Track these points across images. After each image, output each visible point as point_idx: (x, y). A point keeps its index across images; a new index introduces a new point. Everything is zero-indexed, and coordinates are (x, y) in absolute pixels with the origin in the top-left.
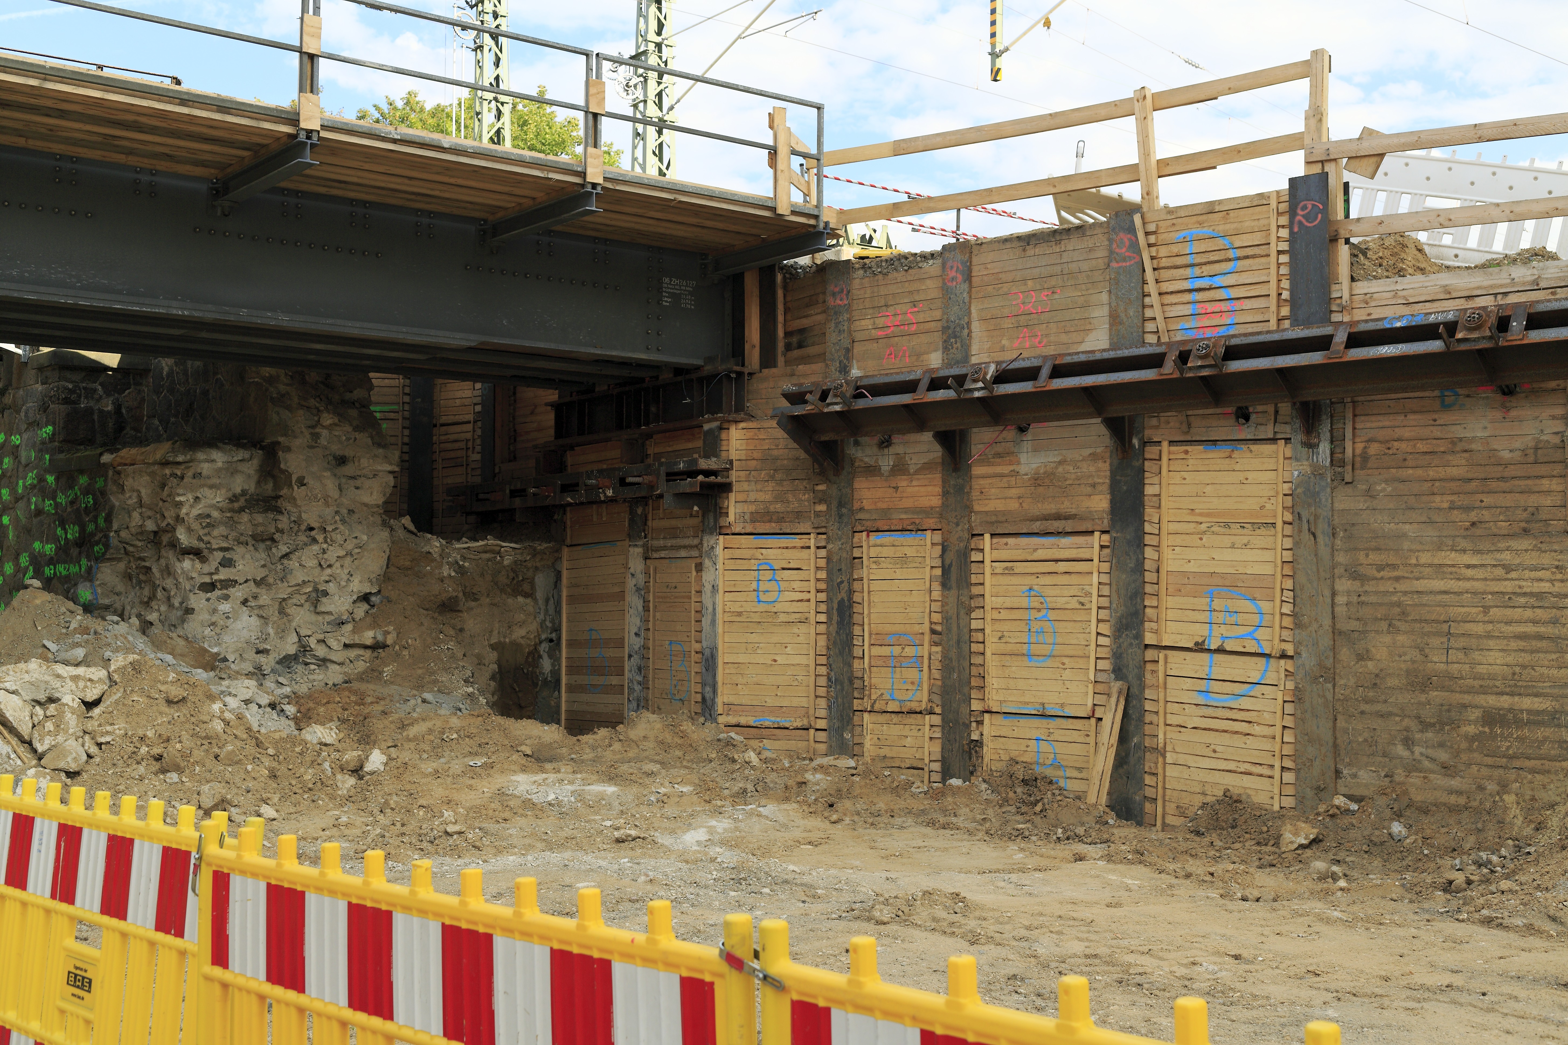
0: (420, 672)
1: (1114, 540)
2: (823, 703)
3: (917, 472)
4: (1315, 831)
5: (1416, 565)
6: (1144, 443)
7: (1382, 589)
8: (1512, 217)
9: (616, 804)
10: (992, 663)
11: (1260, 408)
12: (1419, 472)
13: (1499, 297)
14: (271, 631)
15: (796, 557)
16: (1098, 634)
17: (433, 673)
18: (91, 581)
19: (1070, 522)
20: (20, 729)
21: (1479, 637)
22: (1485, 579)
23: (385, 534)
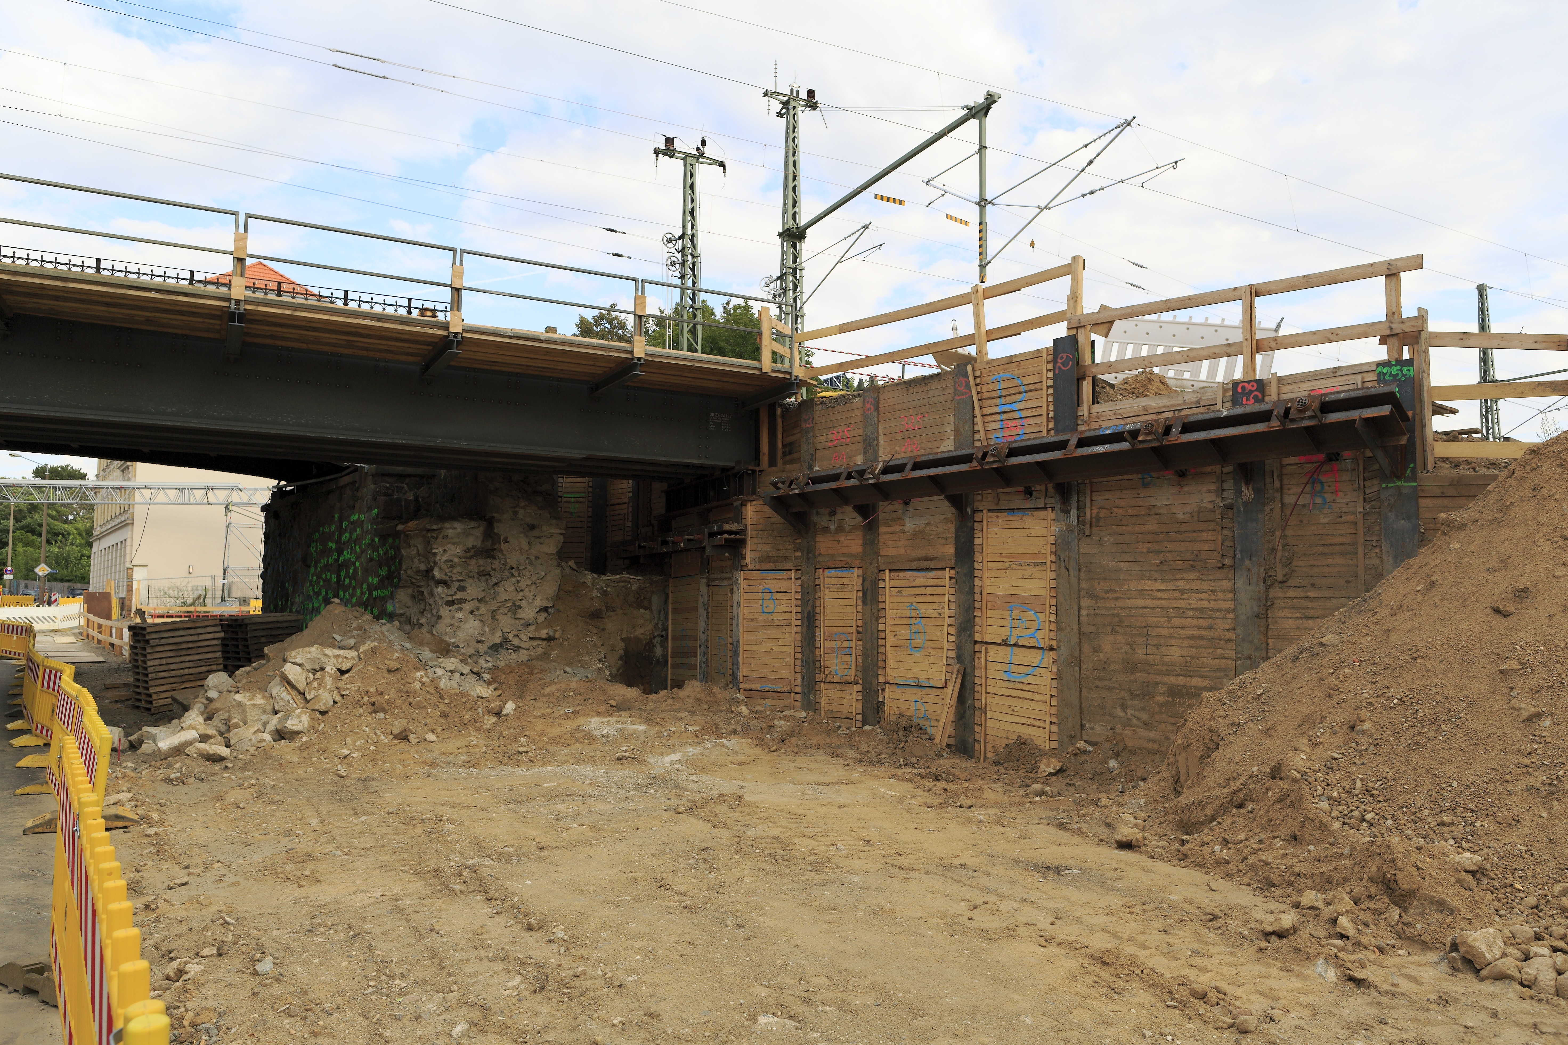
0: (573, 654)
1: (957, 573)
2: (799, 676)
3: (850, 531)
4: (1060, 764)
5: (1128, 590)
6: (975, 511)
7: (1108, 605)
8: (1188, 360)
9: (642, 738)
10: (890, 652)
11: (1038, 487)
12: (1130, 528)
13: (1176, 412)
14: (487, 629)
15: (784, 585)
16: (948, 634)
17: (580, 656)
18: (393, 599)
19: (933, 562)
20: (298, 686)
21: (1165, 637)
22: (1169, 599)
23: (558, 571)
